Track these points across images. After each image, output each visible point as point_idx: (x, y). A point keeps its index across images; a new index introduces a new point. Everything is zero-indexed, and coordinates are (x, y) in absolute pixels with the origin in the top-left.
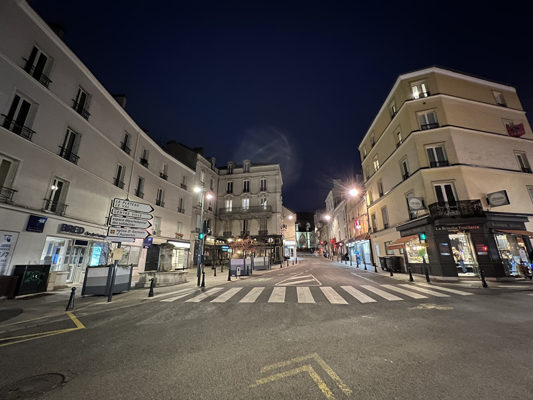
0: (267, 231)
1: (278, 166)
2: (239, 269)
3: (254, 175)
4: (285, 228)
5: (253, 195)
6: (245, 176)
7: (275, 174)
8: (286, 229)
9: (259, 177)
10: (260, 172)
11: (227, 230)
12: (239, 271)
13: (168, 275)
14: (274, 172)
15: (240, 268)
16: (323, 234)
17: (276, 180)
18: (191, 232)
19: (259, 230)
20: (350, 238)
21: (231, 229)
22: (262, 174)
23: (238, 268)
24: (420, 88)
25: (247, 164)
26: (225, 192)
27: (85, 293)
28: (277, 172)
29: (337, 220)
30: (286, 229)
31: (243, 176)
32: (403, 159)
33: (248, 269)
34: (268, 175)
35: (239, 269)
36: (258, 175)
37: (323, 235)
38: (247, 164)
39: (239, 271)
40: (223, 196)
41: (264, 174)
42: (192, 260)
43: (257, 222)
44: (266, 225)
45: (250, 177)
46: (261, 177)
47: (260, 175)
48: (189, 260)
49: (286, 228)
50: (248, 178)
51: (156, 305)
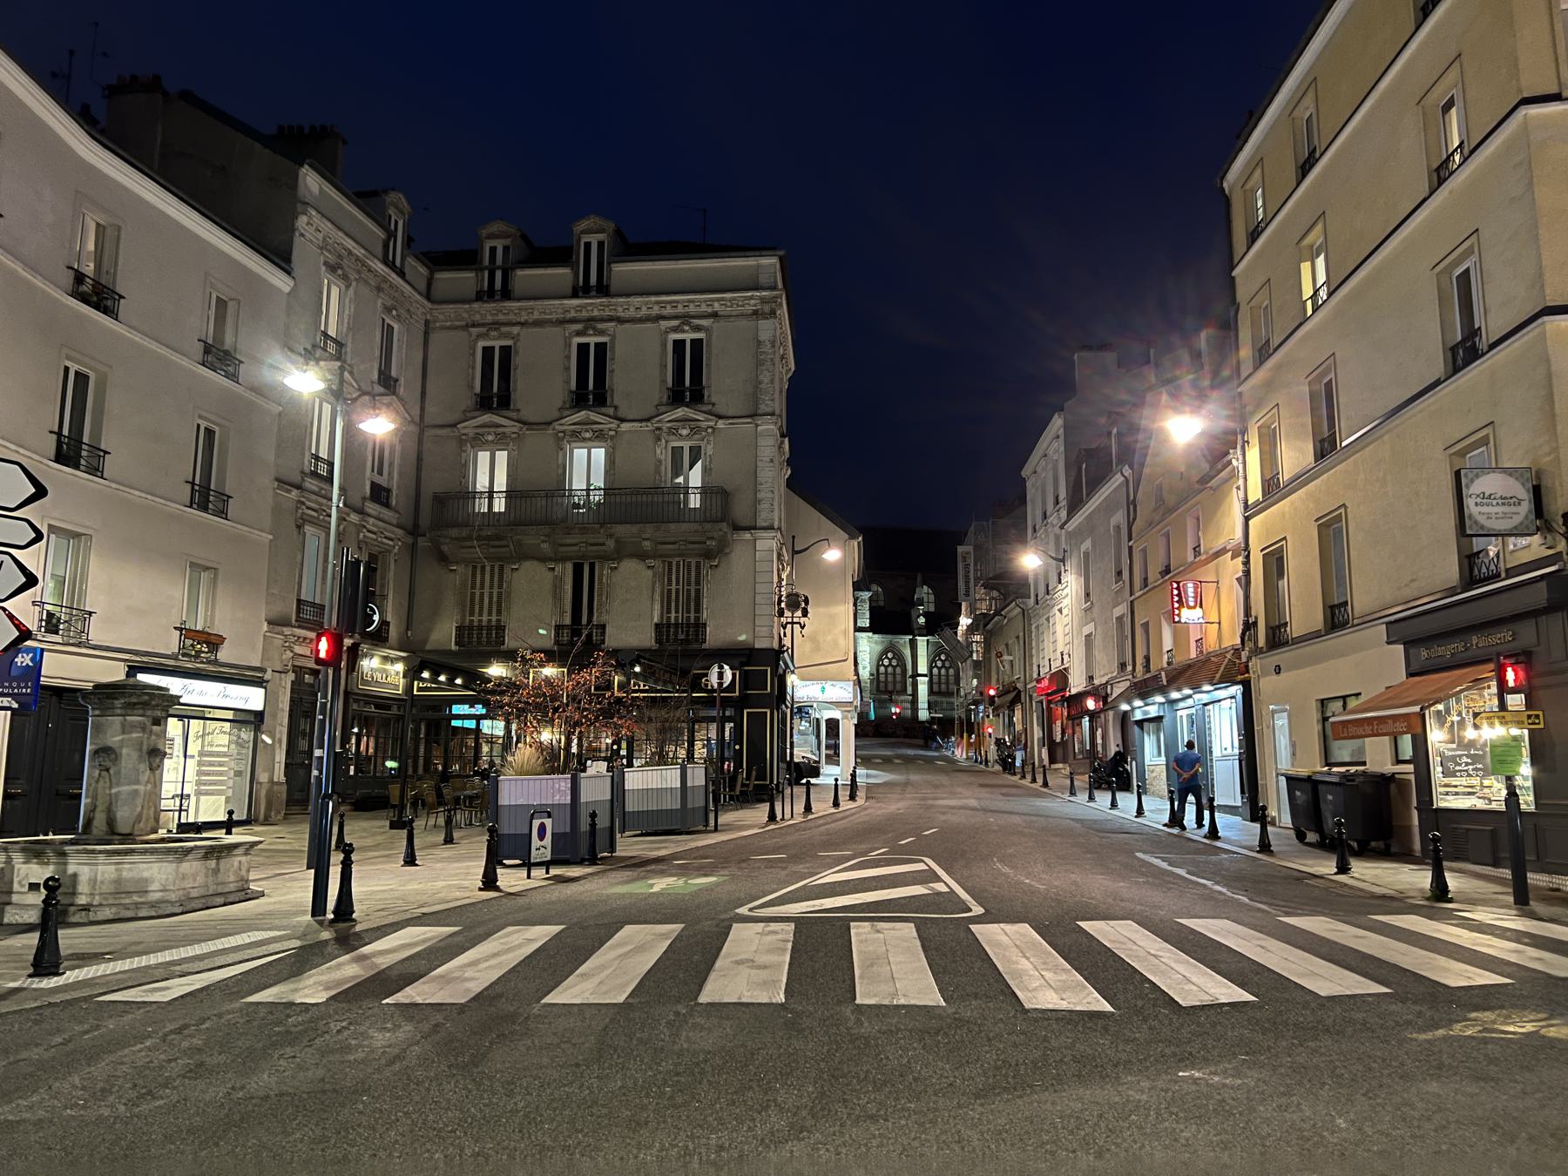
2: (542, 827)
4: (799, 613)
8: (803, 620)
11: (476, 618)
12: (542, 836)
15: (548, 822)
16: (1001, 648)
17: (759, 343)
18: (270, 623)
21: (499, 612)
23: (536, 823)
26: (468, 402)
30: (803, 620)
33: (593, 825)
35: (542, 827)
37: (999, 655)
39: (542, 836)
40: (454, 425)
42: (279, 774)
44: (698, 591)
48: (263, 777)
49: (805, 613)
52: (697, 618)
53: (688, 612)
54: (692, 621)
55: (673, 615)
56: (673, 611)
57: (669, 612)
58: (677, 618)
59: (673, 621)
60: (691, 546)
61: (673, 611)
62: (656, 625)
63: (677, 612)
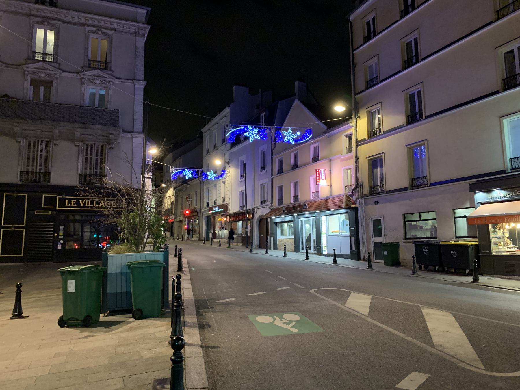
0: (47, 174)
1: (142, 12)
3: (69, 19)
5: (64, 74)
6: (42, 14)
7: (135, 33)
9: (87, 28)
10: (90, 13)
13: (434, 189)
14: (134, 27)
17: (136, 47)
19: (79, 172)
20: (276, 204)
22: (96, 23)
24: (108, 237)
25: (90, 145)
27: (68, 242)
28: (139, 28)
29: (349, 122)
31: (34, 12)
32: (378, 68)
34: (115, 30)
36: (83, 20)
38: (90, 145)
41: (102, 24)
43: (76, 149)
45: (58, 20)
46: (94, 29)
47: (90, 22)
50: (51, 21)
51: (125, 231)
52: (45, 170)
53: (97, 169)
54: (88, 173)
55: (88, 170)
56: (31, 164)
57: (86, 168)
58: (90, 172)
59: (88, 173)
60: (99, 137)
61: (31, 164)
62: (80, 174)
63: (90, 169)
